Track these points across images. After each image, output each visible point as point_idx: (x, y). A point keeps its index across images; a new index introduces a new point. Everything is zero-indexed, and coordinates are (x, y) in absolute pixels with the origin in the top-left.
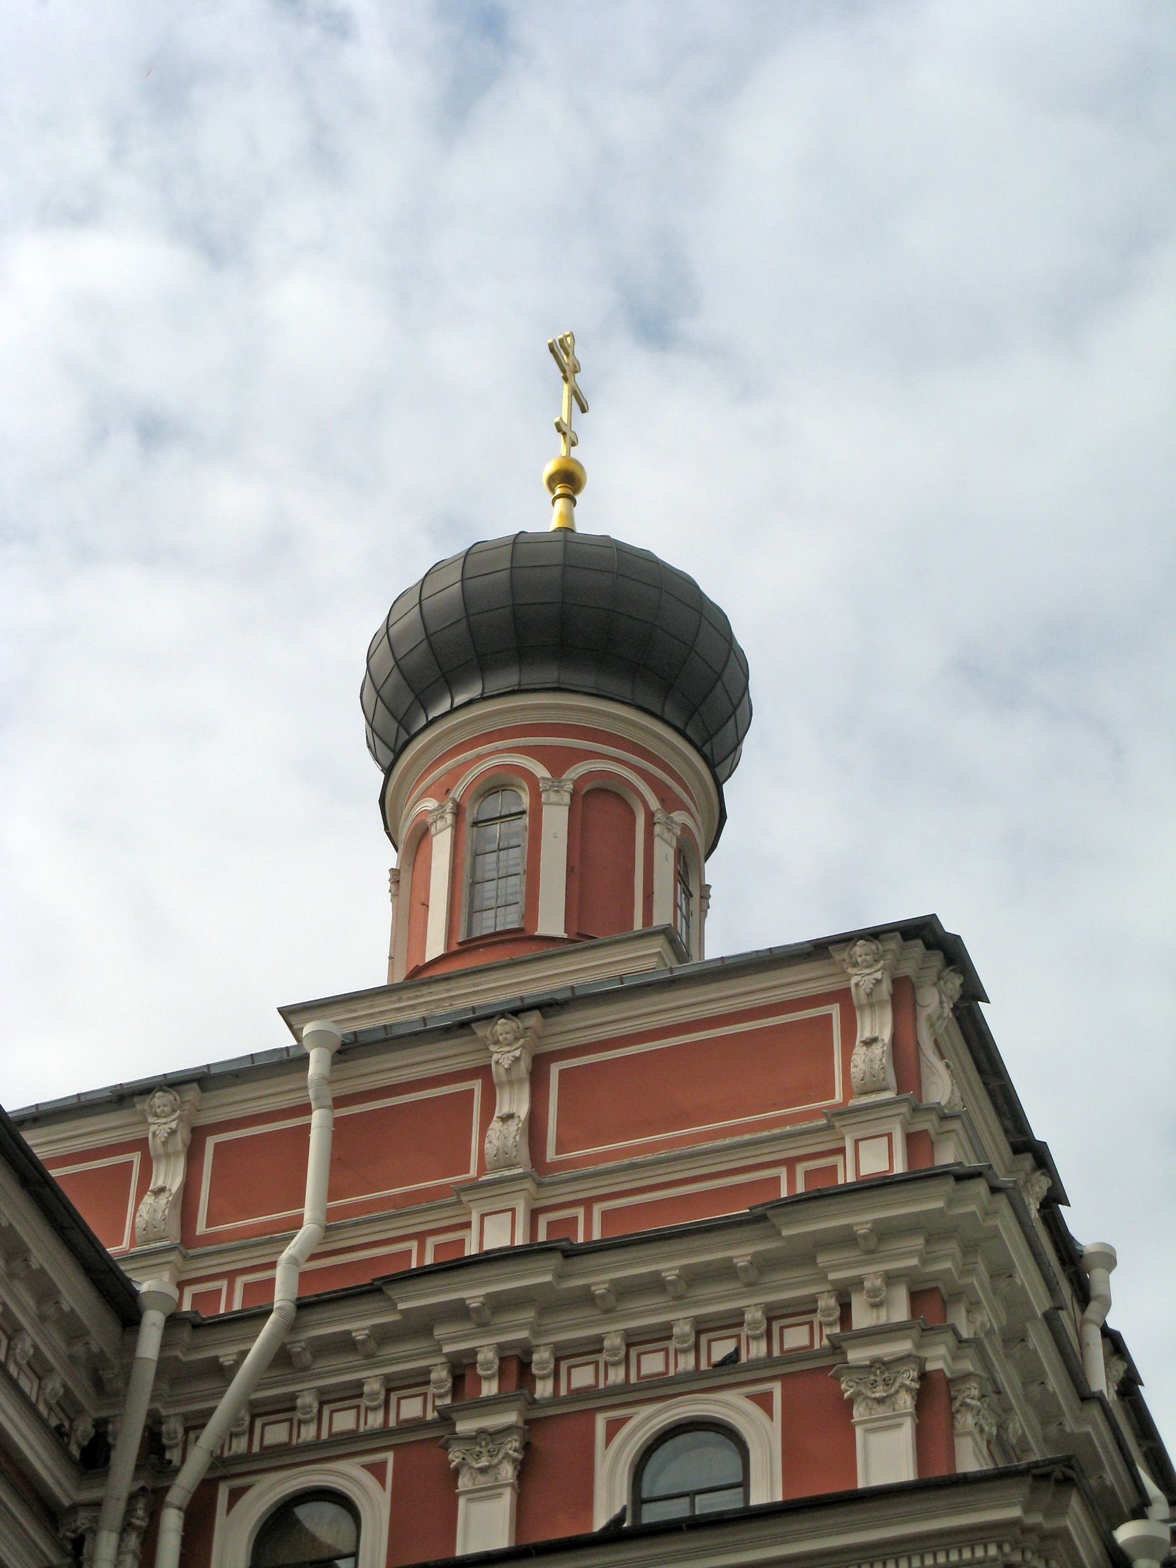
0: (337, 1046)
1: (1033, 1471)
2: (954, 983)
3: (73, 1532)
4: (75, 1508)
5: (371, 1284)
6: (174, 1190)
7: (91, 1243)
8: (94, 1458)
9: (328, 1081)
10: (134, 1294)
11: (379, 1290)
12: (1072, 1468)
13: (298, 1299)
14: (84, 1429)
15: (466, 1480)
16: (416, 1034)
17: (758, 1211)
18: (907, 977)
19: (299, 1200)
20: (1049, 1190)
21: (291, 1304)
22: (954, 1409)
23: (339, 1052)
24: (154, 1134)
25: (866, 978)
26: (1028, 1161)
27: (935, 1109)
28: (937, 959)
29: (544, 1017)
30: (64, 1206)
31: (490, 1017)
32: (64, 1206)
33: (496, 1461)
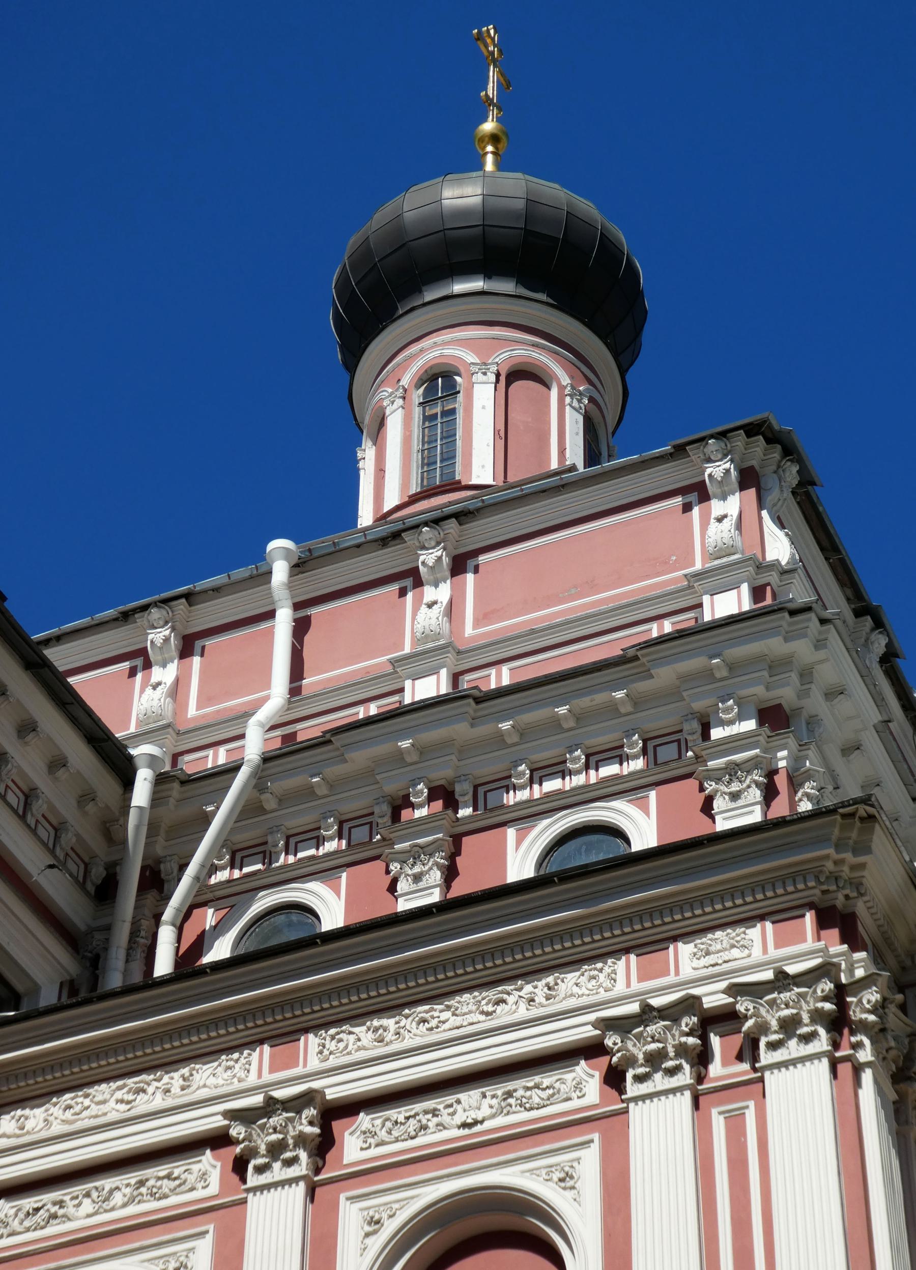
0: (295, 560)
3: (90, 952)
4: (91, 931)
5: (322, 737)
6: (168, 685)
7: (90, 716)
8: (106, 892)
10: (130, 758)
11: (329, 742)
12: (872, 806)
13: (263, 753)
14: (98, 873)
15: (403, 884)
16: (358, 546)
17: (631, 653)
18: (752, 467)
20: (887, 646)
21: (259, 758)
22: (797, 799)
24: (152, 642)
25: (717, 469)
26: (868, 621)
27: (775, 564)
28: (776, 453)
30: (7, 620)
31: (416, 527)
32: (7, 620)
33: (427, 868)
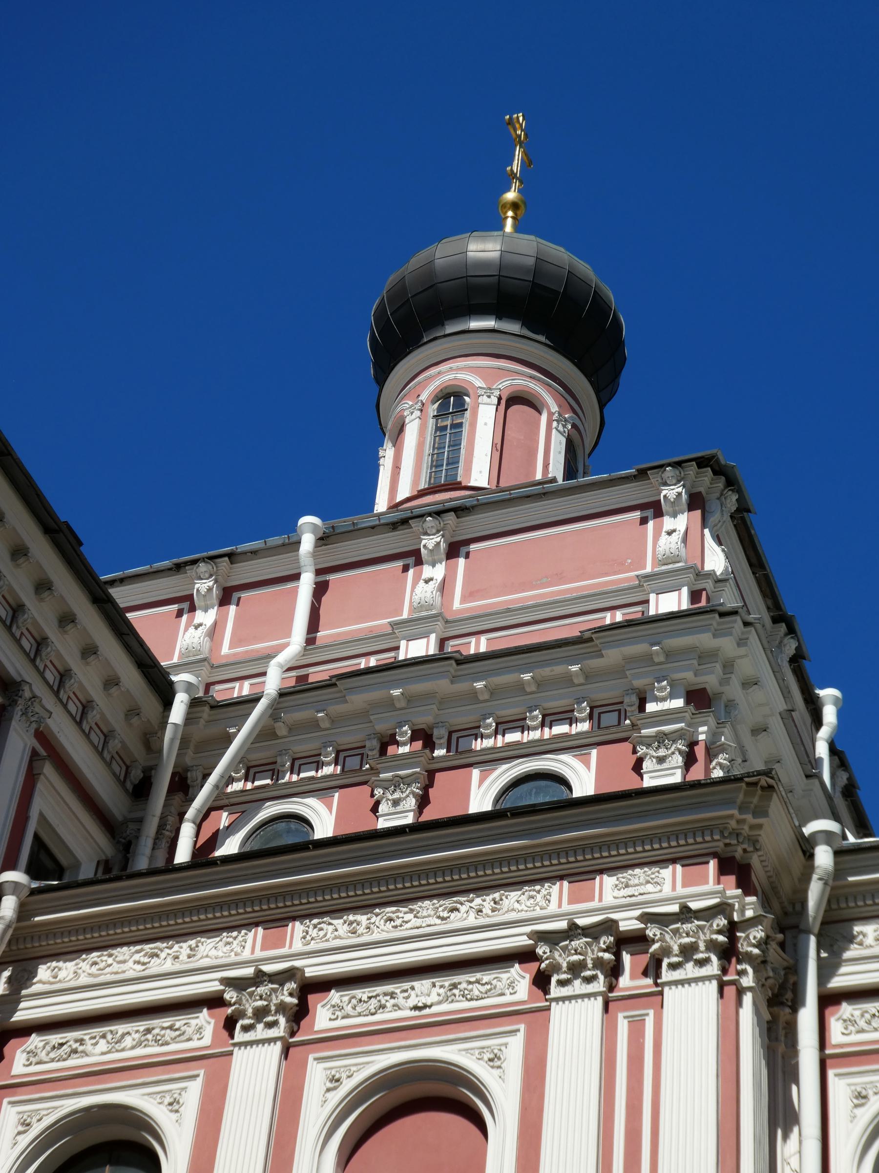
0: (320, 535)
1: (746, 779)
2: (732, 499)
4: (126, 822)
6: (208, 626)
8: (141, 791)
9: (315, 554)
12: (772, 778)
14: (137, 774)
16: (373, 527)
19: (288, 634)
23: (321, 539)
24: (198, 590)
26: (783, 628)
29: (458, 518)
31: (422, 516)
33: (405, 795)
